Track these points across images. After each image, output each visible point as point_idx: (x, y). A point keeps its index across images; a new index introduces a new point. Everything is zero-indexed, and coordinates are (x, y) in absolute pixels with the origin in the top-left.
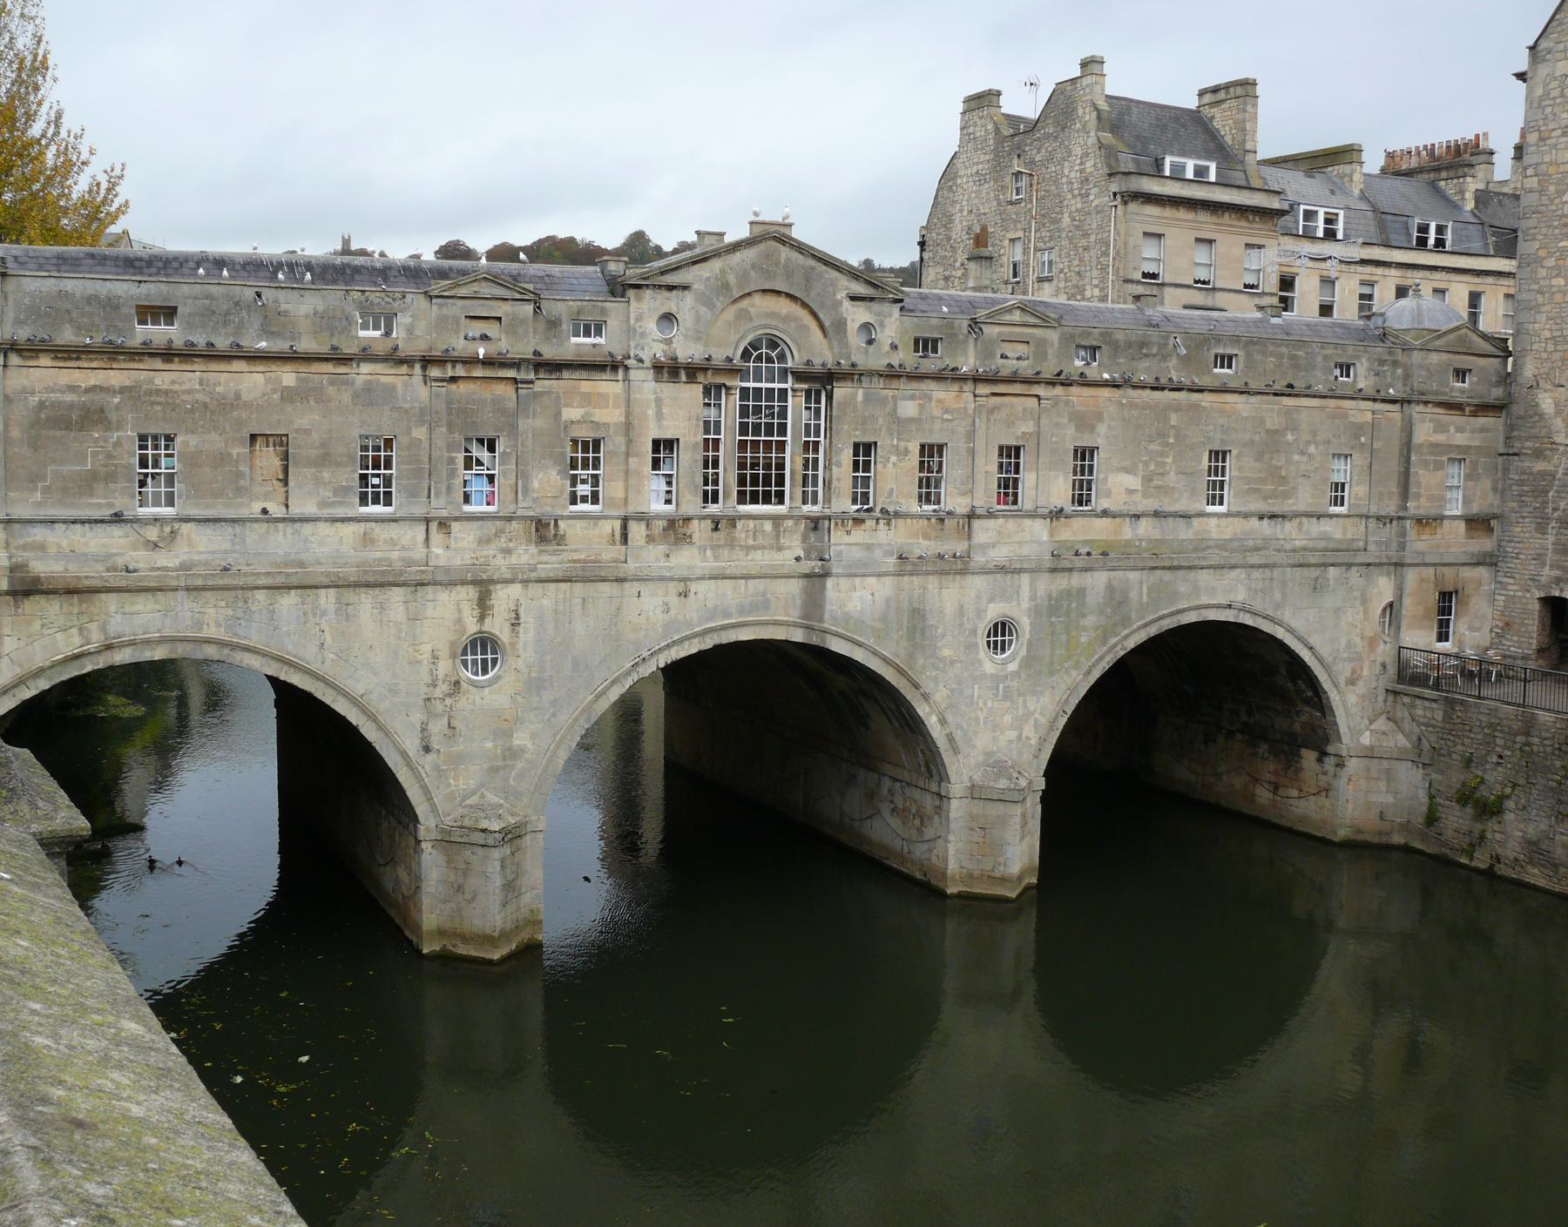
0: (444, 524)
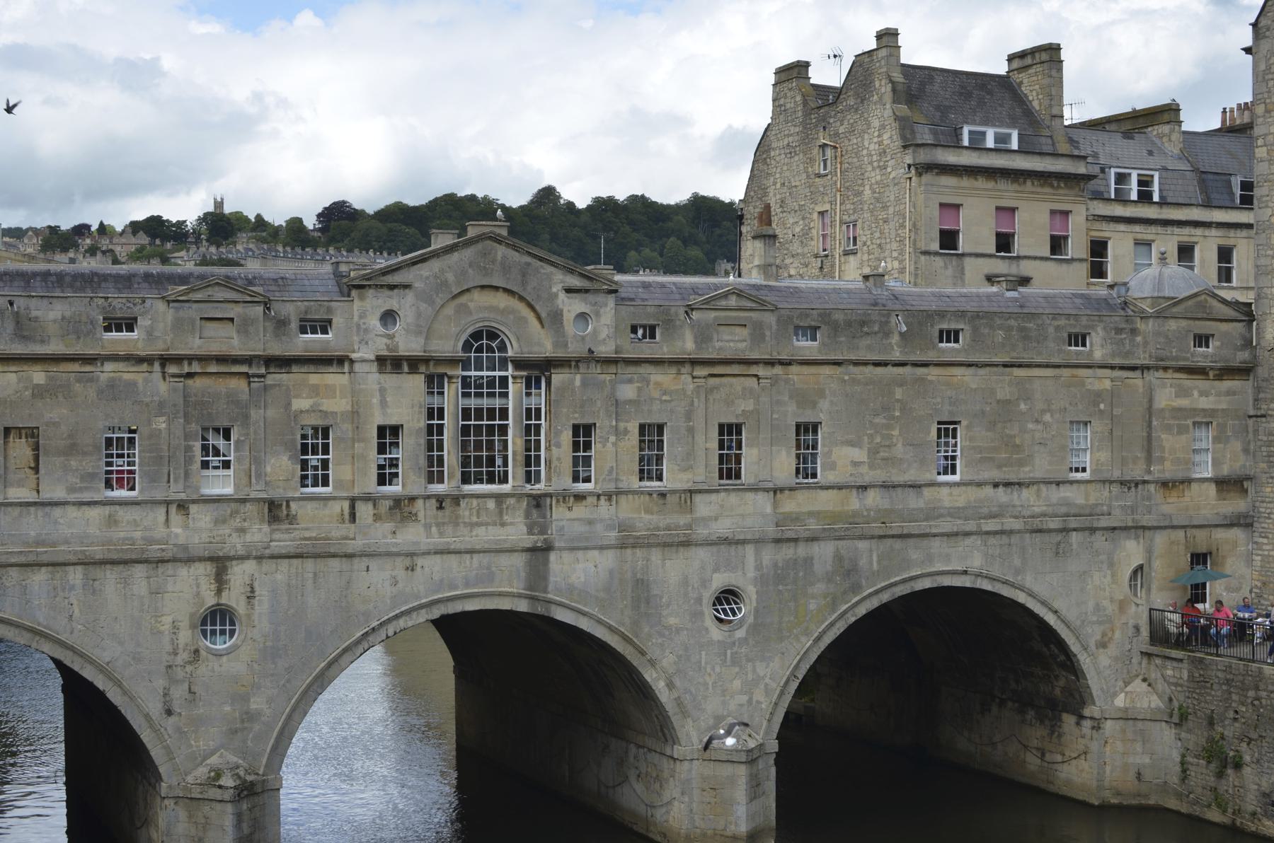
0: (183, 506)
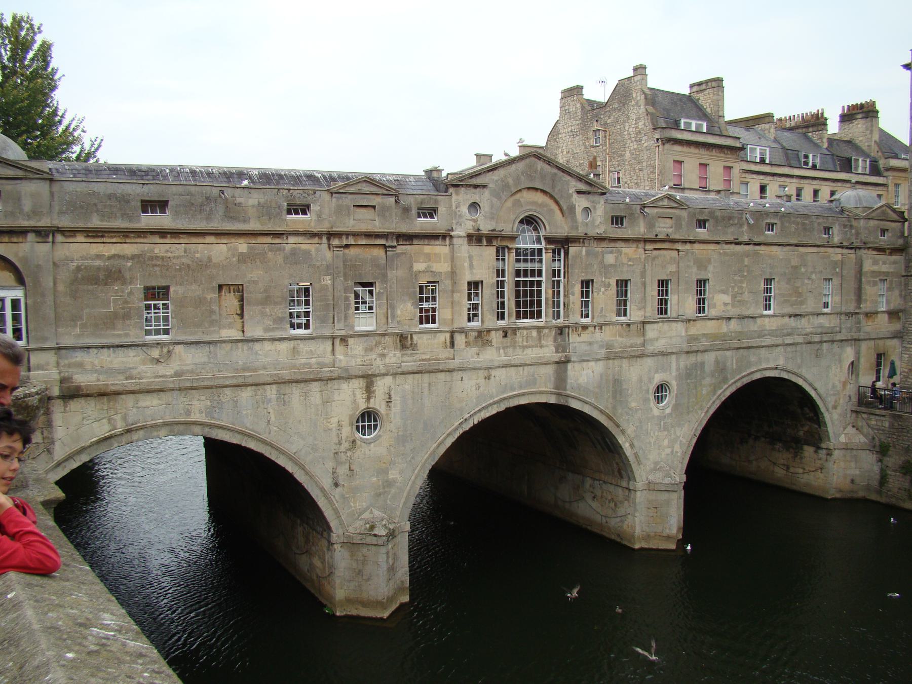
0: (344, 340)
